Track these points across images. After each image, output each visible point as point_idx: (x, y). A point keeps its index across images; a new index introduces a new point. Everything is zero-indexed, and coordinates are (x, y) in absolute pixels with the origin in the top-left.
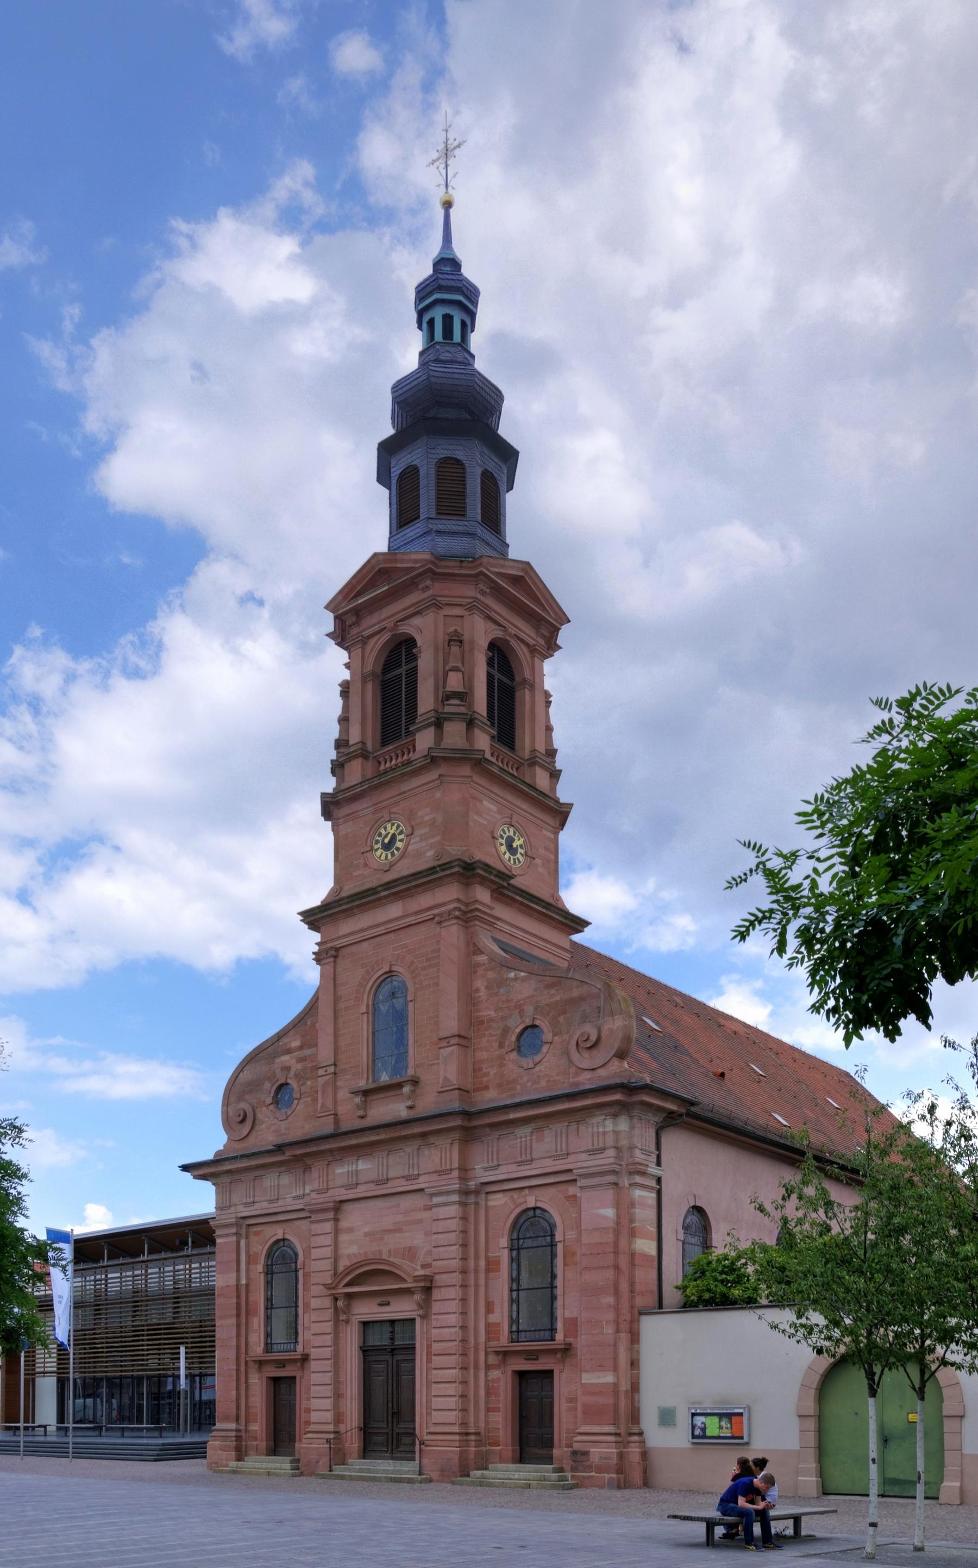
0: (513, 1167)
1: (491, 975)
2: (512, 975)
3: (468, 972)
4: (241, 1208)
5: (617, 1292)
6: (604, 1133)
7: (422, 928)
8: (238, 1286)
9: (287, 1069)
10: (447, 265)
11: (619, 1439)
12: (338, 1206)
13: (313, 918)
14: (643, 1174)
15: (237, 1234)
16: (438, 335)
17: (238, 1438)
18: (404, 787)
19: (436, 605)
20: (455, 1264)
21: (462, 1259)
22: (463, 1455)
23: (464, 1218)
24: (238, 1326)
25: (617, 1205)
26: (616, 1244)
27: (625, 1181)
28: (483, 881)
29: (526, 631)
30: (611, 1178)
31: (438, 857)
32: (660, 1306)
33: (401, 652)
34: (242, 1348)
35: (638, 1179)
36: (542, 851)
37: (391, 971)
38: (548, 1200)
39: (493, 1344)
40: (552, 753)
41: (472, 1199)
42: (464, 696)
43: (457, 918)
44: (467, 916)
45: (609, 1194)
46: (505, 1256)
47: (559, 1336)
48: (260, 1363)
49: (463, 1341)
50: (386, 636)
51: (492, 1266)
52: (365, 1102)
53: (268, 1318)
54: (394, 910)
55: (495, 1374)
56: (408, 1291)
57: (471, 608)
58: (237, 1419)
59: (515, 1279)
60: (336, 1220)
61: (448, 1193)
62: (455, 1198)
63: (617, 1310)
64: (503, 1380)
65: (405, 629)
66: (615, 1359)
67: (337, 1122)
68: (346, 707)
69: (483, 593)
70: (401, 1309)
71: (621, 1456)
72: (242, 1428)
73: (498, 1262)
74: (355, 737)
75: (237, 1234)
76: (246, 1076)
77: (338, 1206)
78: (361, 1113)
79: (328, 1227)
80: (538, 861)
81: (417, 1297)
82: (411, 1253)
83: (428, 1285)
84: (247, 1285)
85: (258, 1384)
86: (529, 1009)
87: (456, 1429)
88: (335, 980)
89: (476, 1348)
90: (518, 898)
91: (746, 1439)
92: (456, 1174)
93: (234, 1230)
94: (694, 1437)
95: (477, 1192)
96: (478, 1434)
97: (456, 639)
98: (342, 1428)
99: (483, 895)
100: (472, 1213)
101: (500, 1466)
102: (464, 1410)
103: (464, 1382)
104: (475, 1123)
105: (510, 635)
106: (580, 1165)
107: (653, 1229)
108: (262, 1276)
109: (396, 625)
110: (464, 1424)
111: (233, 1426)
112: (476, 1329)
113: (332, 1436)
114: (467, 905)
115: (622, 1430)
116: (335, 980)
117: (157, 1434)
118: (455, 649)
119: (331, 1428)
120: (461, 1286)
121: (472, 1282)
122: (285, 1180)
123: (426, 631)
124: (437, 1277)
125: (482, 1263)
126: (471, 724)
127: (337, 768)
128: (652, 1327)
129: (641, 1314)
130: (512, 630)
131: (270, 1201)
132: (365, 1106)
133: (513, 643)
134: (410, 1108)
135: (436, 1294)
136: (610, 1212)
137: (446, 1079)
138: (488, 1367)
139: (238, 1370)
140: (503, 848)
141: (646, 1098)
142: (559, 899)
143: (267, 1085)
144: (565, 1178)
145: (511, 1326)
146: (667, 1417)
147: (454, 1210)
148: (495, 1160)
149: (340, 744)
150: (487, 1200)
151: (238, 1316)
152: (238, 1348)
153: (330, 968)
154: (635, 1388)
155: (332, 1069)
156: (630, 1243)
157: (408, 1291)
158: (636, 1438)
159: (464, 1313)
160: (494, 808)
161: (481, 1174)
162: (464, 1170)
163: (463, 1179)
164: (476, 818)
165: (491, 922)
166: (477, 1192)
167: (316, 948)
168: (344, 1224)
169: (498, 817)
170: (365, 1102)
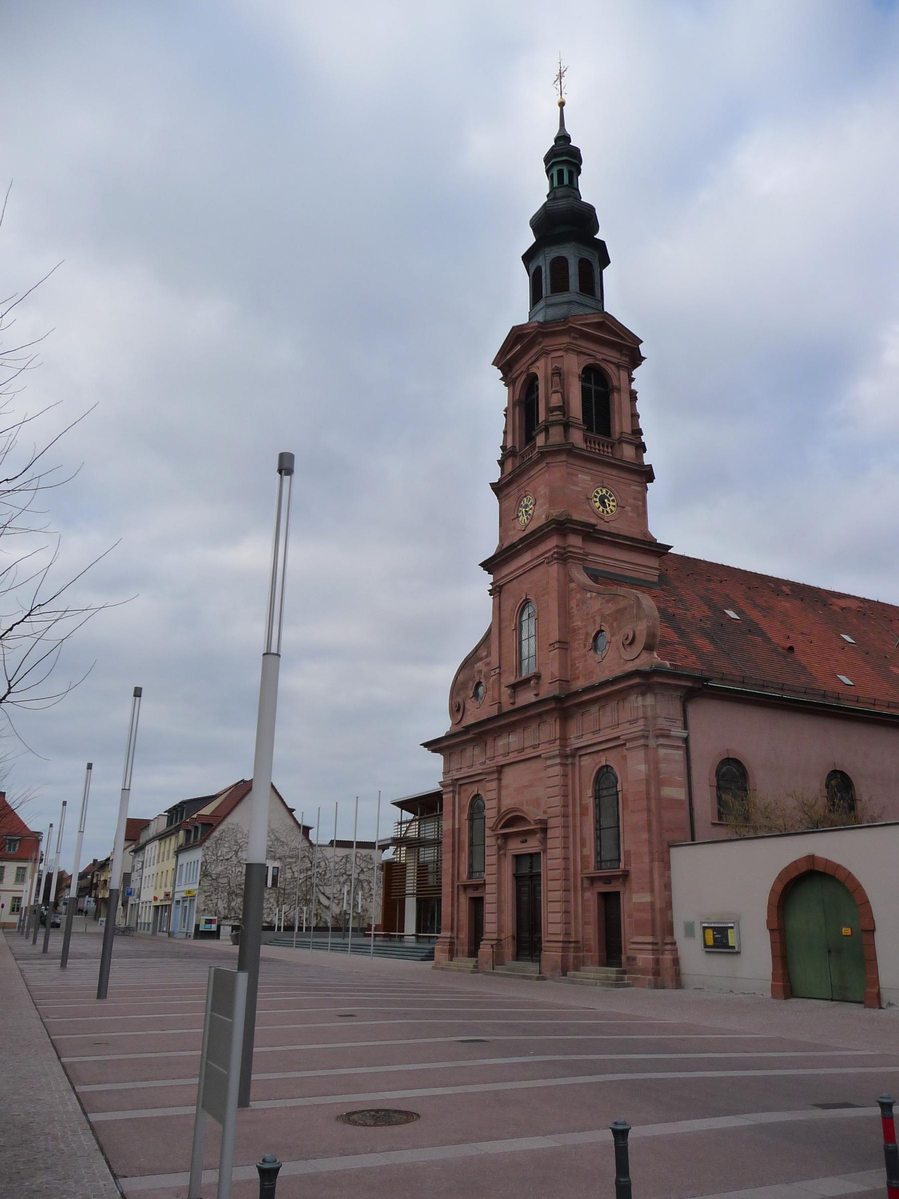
0: (590, 736)
1: (579, 596)
2: (589, 595)
3: (564, 598)
4: (454, 773)
5: (650, 830)
6: (637, 707)
7: (541, 568)
8: (453, 830)
9: (480, 672)
10: (563, 138)
11: (655, 947)
12: (500, 769)
13: (489, 565)
14: (668, 736)
15: (453, 792)
16: (555, 184)
17: (452, 944)
18: (532, 473)
19: (546, 353)
20: (558, 810)
21: (563, 806)
22: (564, 959)
23: (565, 775)
24: (453, 859)
25: (647, 762)
26: (648, 793)
27: (652, 743)
28: (575, 532)
29: (612, 355)
30: (642, 742)
31: (547, 517)
32: (692, 839)
33: (531, 382)
34: (456, 875)
35: (662, 741)
36: (631, 501)
37: (526, 599)
38: (610, 759)
39: (585, 871)
40: (639, 432)
41: (570, 761)
42: (563, 408)
43: (556, 559)
44: (563, 557)
45: (641, 754)
46: (590, 803)
47: (622, 865)
48: (466, 887)
49: (566, 869)
50: (524, 377)
51: (584, 811)
52: (514, 692)
53: (471, 853)
54: (526, 557)
55: (588, 895)
56: (532, 832)
57: (567, 350)
58: (452, 929)
59: (598, 821)
60: (499, 779)
61: (554, 757)
62: (558, 761)
63: (650, 842)
64: (591, 897)
65: (533, 370)
66: (652, 883)
67: (500, 708)
68: (633, 407)
69: (574, 338)
70: (532, 845)
71: (657, 962)
72: (455, 935)
73: (587, 809)
74: (509, 445)
75: (453, 792)
76: (461, 677)
77: (500, 769)
78: (512, 701)
79: (494, 785)
80: (628, 508)
81: (538, 836)
82: (537, 803)
83: (544, 826)
84: (459, 829)
85: (464, 901)
86: (598, 619)
87: (560, 938)
88: (500, 608)
89: (575, 874)
90: (605, 537)
91: (736, 949)
92: (558, 742)
93: (451, 789)
94: (706, 946)
95: (573, 756)
96: (577, 942)
97: (558, 372)
98: (503, 937)
99: (575, 541)
100: (570, 772)
101: (591, 967)
102: (567, 923)
103: (567, 901)
104: (566, 705)
105: (599, 360)
106: (625, 732)
107: (682, 779)
108: (591, 799)
109: (528, 369)
110: (567, 934)
111: (449, 934)
112: (575, 860)
113: (495, 942)
114: (564, 548)
115: (659, 941)
116: (500, 608)
117: (427, 940)
118: (556, 379)
119: (495, 936)
120: (564, 827)
121: (571, 824)
122: (477, 751)
123: (541, 369)
124: (550, 821)
125: (578, 809)
126: (567, 426)
127: (501, 463)
128: (679, 856)
129: (671, 846)
130: (600, 357)
131: (469, 767)
132: (514, 695)
133: (603, 365)
134: (537, 695)
135: (550, 833)
136: (642, 768)
137: (552, 674)
138: (583, 890)
139: (453, 892)
140: (598, 504)
141: (660, 680)
142: (647, 533)
143: (471, 683)
144: (618, 744)
145: (596, 858)
146: (689, 930)
147: (557, 770)
148: (584, 731)
149: (503, 448)
150: (580, 761)
151: (453, 851)
152: (453, 876)
153: (497, 599)
154: (669, 905)
155: (497, 671)
156: (658, 791)
157: (532, 832)
158: (669, 947)
159: (566, 848)
160: (588, 478)
161: (575, 743)
162: (564, 739)
163: (563, 746)
164: (573, 487)
165: (582, 559)
166: (573, 756)
167: (491, 587)
168: (504, 782)
169: (591, 483)
170: (514, 692)
